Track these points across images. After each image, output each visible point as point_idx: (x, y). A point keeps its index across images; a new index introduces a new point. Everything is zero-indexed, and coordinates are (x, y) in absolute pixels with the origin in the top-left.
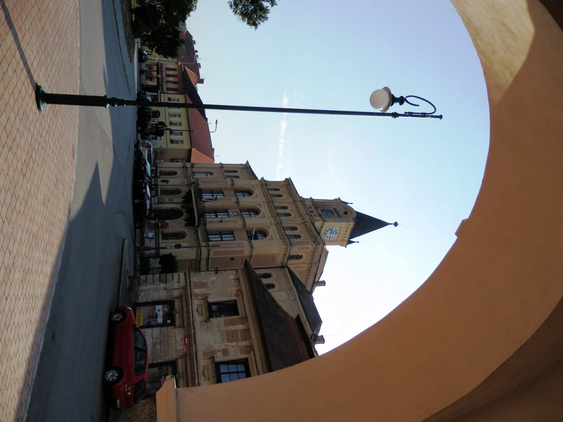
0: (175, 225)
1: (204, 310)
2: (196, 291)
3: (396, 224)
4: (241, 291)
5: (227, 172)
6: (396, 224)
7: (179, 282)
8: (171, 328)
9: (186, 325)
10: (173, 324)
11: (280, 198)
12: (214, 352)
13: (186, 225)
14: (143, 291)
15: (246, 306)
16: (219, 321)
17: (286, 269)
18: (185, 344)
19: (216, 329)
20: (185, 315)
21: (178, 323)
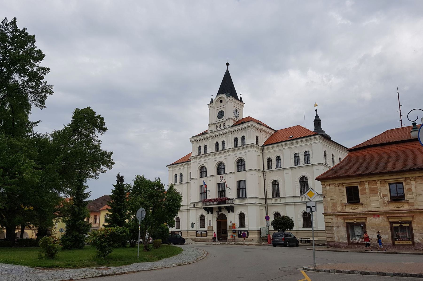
0: (232, 219)
1: (356, 206)
2: (339, 209)
3: (228, 64)
4: (339, 184)
5: (176, 182)
6: (228, 64)
7: (332, 219)
8: (367, 224)
9: (364, 216)
10: (364, 223)
11: (208, 146)
12: (384, 201)
13: (233, 211)
14: (339, 239)
15: (352, 182)
16: (362, 198)
17: (265, 147)
18: (379, 217)
19: (368, 199)
20: (358, 216)
21: (364, 221)
